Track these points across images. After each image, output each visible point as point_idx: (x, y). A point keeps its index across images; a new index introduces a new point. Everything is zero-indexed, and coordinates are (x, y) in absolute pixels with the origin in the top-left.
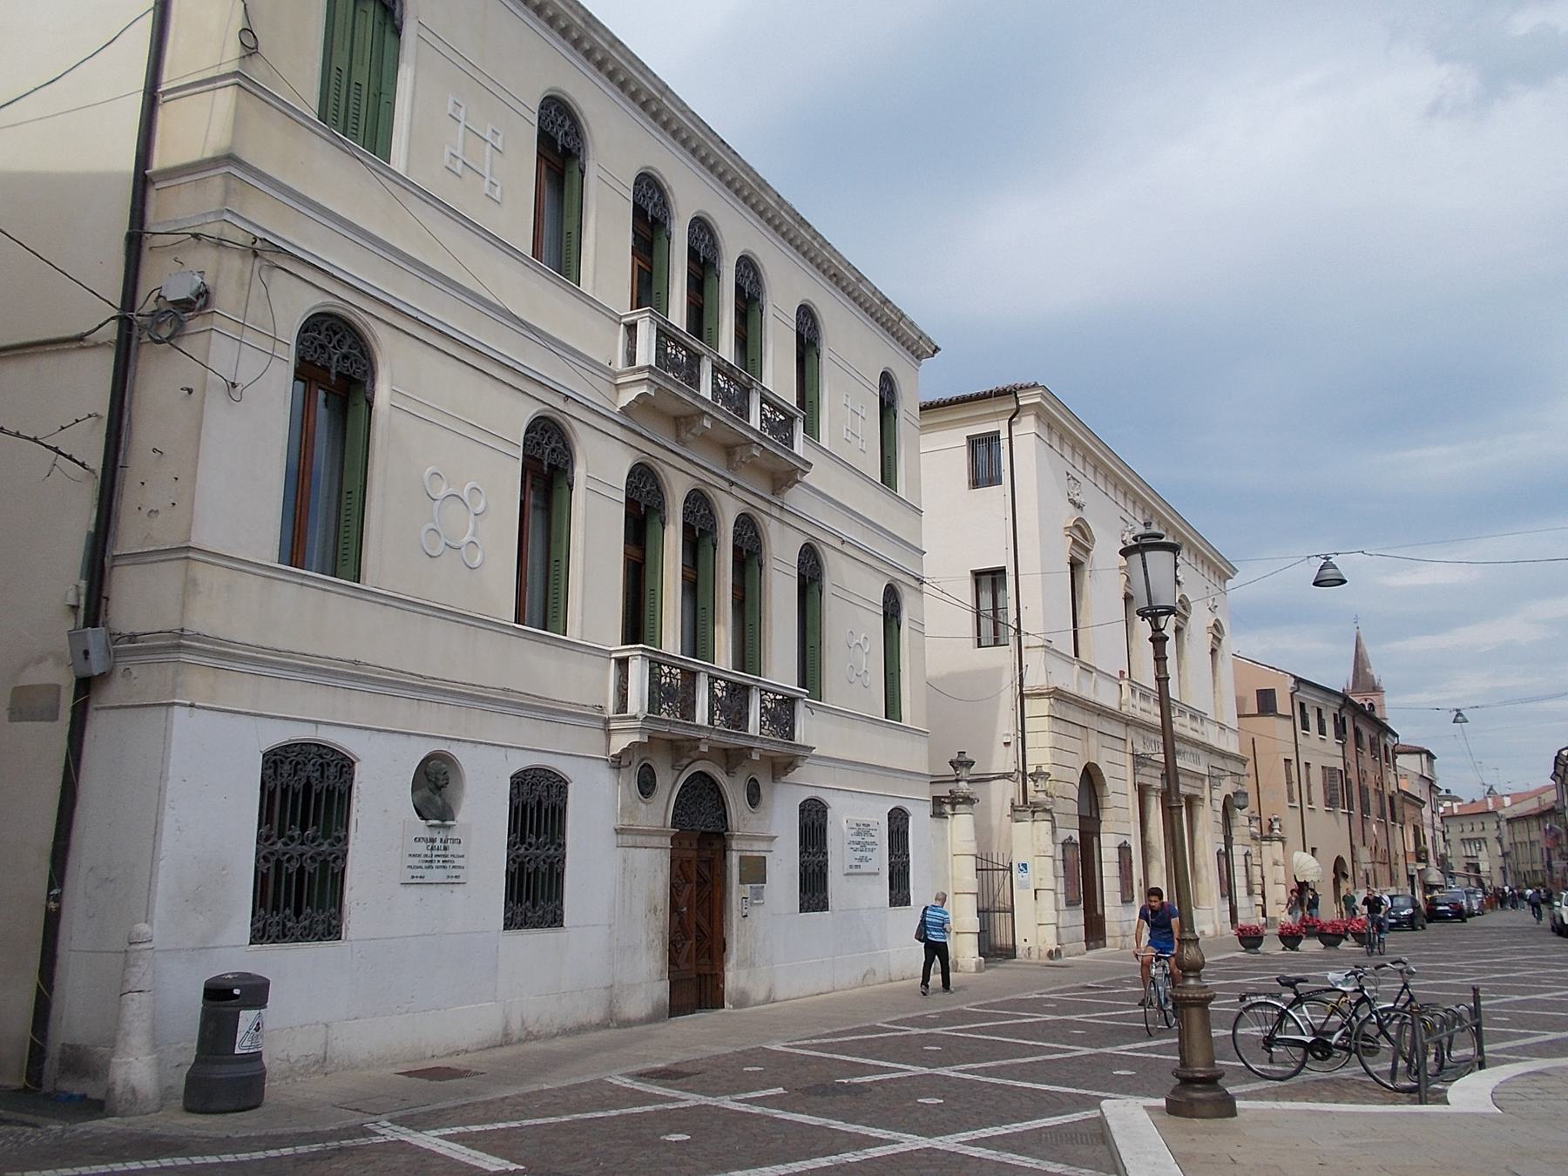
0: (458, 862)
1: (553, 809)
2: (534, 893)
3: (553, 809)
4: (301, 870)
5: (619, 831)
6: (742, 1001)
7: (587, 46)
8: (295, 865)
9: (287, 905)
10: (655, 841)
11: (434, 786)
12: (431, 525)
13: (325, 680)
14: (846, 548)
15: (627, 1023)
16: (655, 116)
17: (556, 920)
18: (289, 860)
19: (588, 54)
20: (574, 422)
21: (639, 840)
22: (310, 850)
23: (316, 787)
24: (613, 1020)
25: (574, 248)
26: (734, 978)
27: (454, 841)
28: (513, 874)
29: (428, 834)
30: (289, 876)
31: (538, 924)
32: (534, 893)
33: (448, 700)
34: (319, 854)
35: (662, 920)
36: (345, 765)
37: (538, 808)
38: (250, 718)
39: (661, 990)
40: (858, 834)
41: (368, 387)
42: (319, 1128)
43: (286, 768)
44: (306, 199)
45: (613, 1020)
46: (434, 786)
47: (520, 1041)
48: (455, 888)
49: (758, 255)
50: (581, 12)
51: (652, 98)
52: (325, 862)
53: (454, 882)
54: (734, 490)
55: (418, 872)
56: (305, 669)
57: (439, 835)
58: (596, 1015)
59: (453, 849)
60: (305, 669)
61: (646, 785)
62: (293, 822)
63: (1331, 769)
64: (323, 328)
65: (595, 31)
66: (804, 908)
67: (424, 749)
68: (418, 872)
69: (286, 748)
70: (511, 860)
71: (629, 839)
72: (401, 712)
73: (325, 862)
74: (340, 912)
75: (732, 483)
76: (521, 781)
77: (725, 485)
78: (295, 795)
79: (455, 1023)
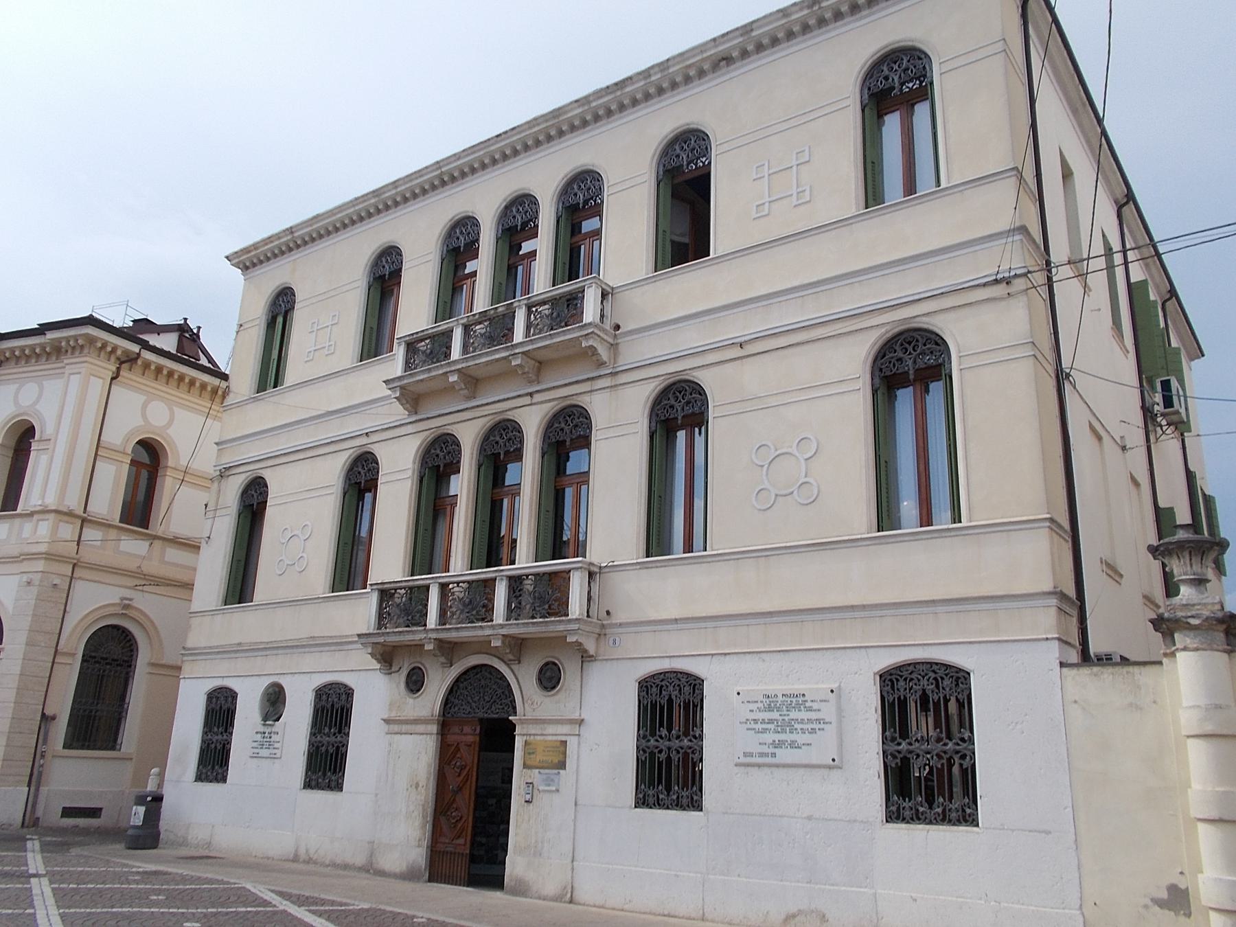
0: (276, 745)
1: (342, 709)
2: (326, 766)
3: (342, 709)
4: (669, 759)
6: (521, 890)
7: (828, 15)
8: (663, 756)
9: (660, 782)
10: (421, 728)
11: (274, 701)
15: (382, 873)
16: (453, 179)
17: (339, 787)
18: (660, 752)
19: (396, 204)
20: (917, 319)
21: (404, 728)
22: (676, 744)
23: (336, 706)
24: (370, 869)
25: (366, 342)
26: (515, 865)
28: (644, 763)
29: (262, 729)
30: (660, 763)
32: (326, 766)
33: (280, 652)
35: (425, 794)
36: (695, 684)
37: (333, 710)
38: (1010, 644)
39: (418, 855)
40: (769, 709)
42: (323, 896)
45: (370, 869)
46: (274, 701)
47: (304, 861)
50: (772, 18)
51: (440, 177)
52: (686, 754)
53: (273, 757)
54: (537, 398)
56: (218, 653)
57: (268, 730)
58: (360, 860)
59: (275, 738)
60: (218, 653)
61: (415, 683)
62: (661, 725)
63: (679, 244)
64: (897, 348)
66: (310, 784)
67: (267, 681)
69: (900, 668)
70: (311, 744)
71: (396, 728)
73: (686, 754)
75: (531, 394)
76: (323, 693)
77: (527, 400)
78: (662, 708)
79: (273, 840)
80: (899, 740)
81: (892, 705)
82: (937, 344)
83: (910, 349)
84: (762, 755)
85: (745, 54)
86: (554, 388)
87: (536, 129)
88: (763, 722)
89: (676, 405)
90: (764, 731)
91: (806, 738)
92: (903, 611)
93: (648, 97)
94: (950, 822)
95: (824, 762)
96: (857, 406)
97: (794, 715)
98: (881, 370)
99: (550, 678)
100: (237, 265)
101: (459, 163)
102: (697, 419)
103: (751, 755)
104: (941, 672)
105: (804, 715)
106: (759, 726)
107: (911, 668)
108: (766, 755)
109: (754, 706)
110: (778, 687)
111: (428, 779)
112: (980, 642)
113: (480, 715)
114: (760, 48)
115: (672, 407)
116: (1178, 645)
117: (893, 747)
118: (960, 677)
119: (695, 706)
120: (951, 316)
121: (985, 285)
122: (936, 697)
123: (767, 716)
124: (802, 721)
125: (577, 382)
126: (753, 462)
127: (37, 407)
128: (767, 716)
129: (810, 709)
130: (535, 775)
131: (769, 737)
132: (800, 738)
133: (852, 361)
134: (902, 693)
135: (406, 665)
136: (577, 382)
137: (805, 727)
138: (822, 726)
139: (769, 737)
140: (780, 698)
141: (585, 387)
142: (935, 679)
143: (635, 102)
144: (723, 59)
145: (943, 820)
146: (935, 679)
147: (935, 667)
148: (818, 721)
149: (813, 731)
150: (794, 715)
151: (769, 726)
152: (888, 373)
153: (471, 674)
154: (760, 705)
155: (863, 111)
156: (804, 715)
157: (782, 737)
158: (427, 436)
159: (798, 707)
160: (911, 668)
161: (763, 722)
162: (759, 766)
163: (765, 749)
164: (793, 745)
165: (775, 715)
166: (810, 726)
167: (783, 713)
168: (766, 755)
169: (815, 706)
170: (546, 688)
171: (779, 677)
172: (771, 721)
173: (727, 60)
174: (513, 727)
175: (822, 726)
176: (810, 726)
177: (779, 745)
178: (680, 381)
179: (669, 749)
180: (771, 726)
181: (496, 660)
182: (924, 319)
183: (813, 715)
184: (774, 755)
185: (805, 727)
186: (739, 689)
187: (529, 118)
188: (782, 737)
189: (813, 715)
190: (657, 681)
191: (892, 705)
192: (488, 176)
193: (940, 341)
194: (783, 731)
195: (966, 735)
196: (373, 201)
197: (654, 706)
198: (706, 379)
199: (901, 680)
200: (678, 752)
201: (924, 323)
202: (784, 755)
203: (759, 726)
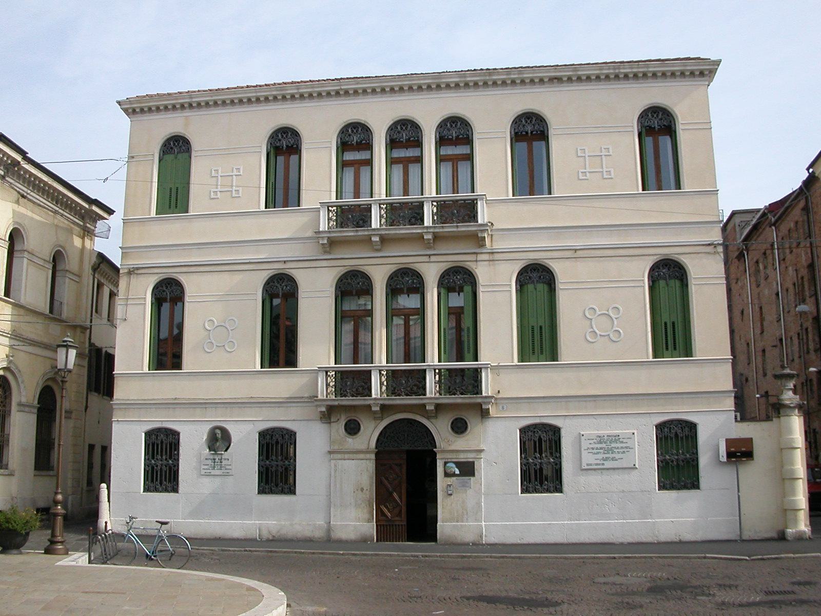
0: (228, 467)
4: (277, 471)
5: (330, 453)
8: (273, 469)
10: (368, 456)
11: (219, 440)
12: (209, 341)
13: (268, 405)
14: (580, 253)
27: (225, 459)
29: (212, 457)
31: (685, 487)
34: (284, 465)
39: (370, 529)
41: (296, 295)
43: (268, 437)
44: (245, 241)
46: (219, 440)
48: (229, 477)
49: (172, 131)
54: (433, 259)
55: (209, 471)
61: (352, 428)
62: (157, 454)
65: (286, 90)
68: (209, 471)
69: (268, 430)
72: (198, 415)
74: (178, 484)
75: (429, 256)
77: (426, 259)
80: (284, 460)
84: (597, 464)
85: (570, 79)
86: (389, 257)
88: (597, 449)
90: (598, 453)
91: (620, 456)
92: (667, 397)
93: (504, 83)
94: (285, 493)
95: (630, 466)
97: (613, 445)
98: (390, 285)
99: (459, 427)
100: (126, 111)
103: (591, 465)
104: (684, 425)
105: (619, 445)
106: (595, 451)
108: (599, 464)
109: (592, 442)
111: (371, 485)
112: (617, 414)
113: (406, 447)
114: (579, 79)
115: (164, 291)
116: (332, 420)
117: (262, 463)
119: (175, 445)
121: (703, 245)
123: (599, 446)
124: (618, 448)
126: (204, 325)
127: (469, 146)
128: (599, 446)
129: (622, 442)
130: (450, 480)
131: (600, 456)
132: (617, 456)
133: (641, 270)
134: (687, 433)
138: (628, 450)
139: (600, 456)
141: (472, 257)
142: (682, 428)
143: (495, 83)
144: (556, 78)
145: (282, 492)
146: (282, 435)
147: (681, 422)
148: (626, 447)
149: (624, 452)
150: (613, 445)
152: (158, 297)
154: (595, 441)
156: (619, 445)
157: (607, 455)
158: (341, 271)
159: (616, 441)
160: (670, 423)
161: (597, 449)
162: (595, 470)
163: (598, 462)
164: (613, 459)
165: (604, 445)
166: (622, 450)
167: (609, 445)
168: (599, 464)
169: (625, 441)
170: (457, 432)
171: (607, 429)
172: (601, 448)
173: (559, 79)
174: (435, 454)
175: (628, 450)
176: (622, 450)
177: (606, 459)
178: (536, 264)
179: (277, 465)
180: (602, 451)
182: (174, 274)
183: (624, 445)
184: (603, 464)
186: (636, 434)
187: (215, 87)
188: (607, 455)
189: (624, 445)
190: (270, 433)
192: (628, 86)
195: (558, 455)
196: (274, 93)
197: (268, 444)
200: (282, 467)
201: (362, 269)
202: (608, 464)
203: (595, 451)
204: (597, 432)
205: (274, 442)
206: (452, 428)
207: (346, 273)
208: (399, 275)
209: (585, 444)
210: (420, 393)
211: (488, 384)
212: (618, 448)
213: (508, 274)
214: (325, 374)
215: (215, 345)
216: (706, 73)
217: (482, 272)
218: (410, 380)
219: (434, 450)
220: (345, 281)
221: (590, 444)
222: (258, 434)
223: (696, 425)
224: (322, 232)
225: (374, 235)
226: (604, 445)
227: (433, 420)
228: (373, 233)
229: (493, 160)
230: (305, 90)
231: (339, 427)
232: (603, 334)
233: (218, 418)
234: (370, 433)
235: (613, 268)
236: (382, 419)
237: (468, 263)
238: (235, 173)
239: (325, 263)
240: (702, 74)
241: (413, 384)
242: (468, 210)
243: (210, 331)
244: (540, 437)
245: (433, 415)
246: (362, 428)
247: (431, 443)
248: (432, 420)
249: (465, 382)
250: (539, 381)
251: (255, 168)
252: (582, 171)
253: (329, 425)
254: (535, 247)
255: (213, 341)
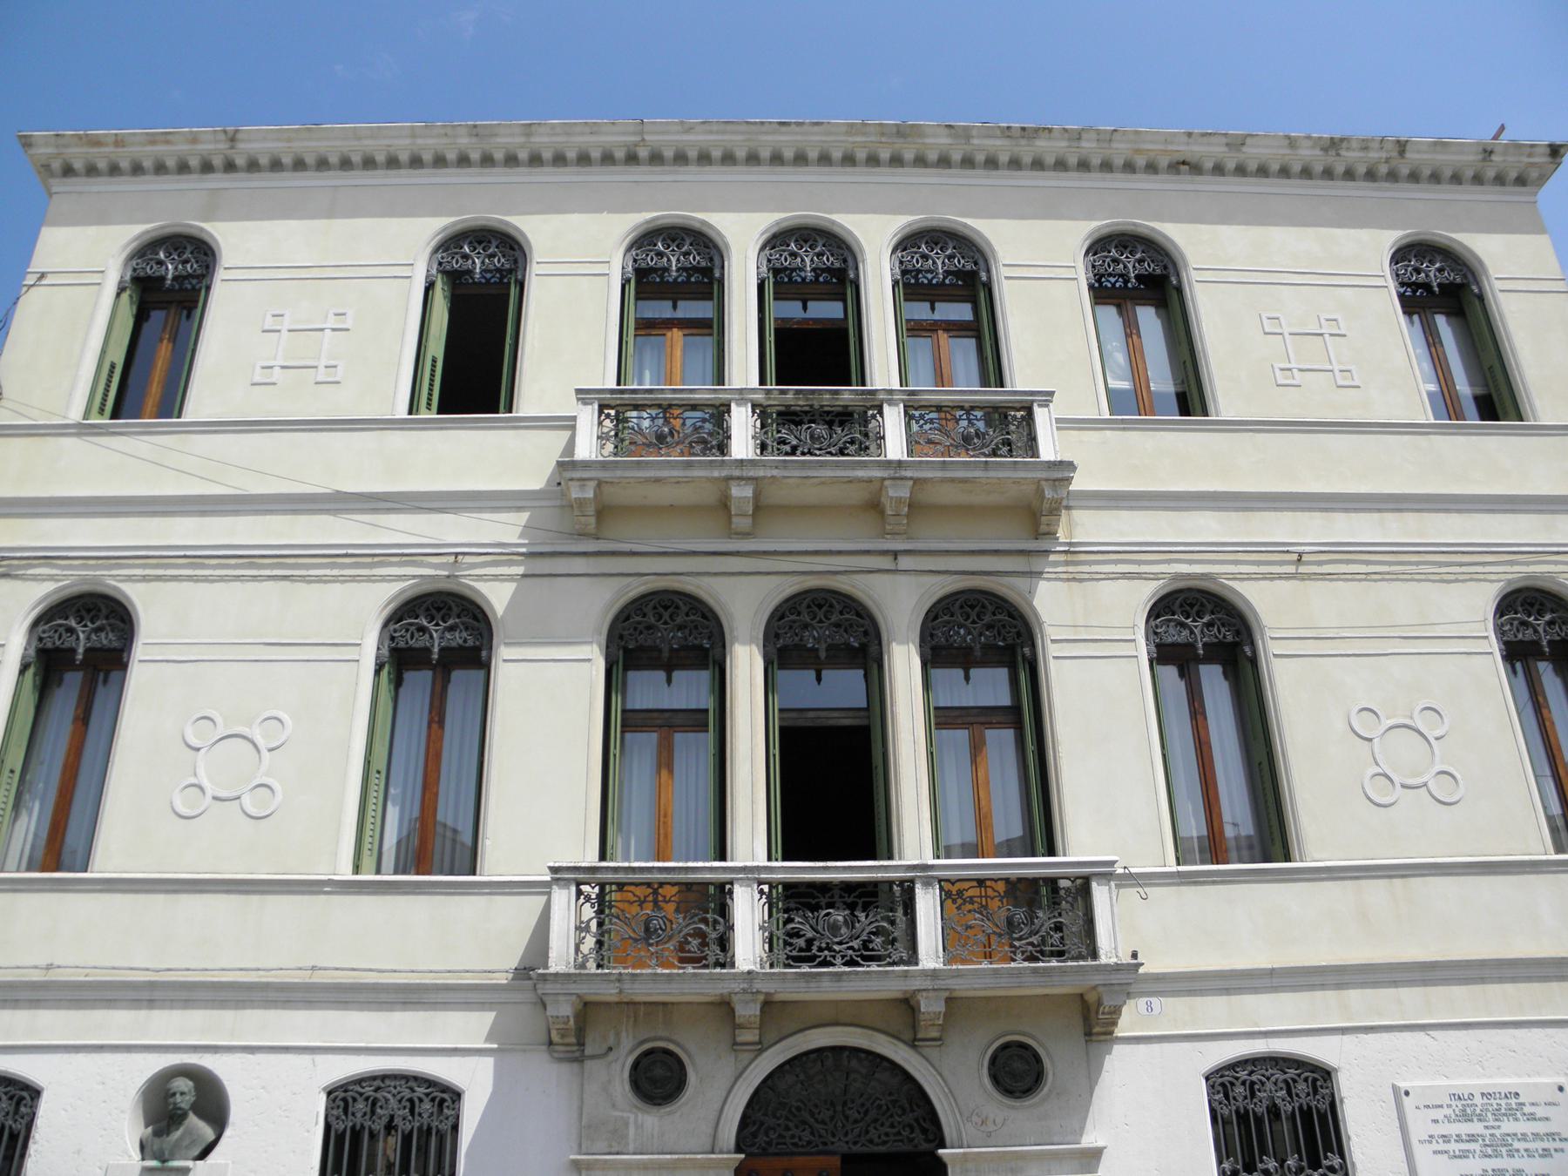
12: (193, 780)
40: (1465, 1117)
54: (905, 562)
61: (658, 1079)
64: (803, 608)
69: (360, 1081)
75: (895, 554)
81: (340, 1138)
82: (704, 617)
83: (666, 616)
87: (859, 139)
88: (1459, 1139)
89: (79, 629)
90: (1464, 1155)
93: (1061, 165)
96: (355, 682)
97: (1508, 1126)
99: (1017, 1072)
101: (685, 137)
102: (109, 662)
105: (1523, 1127)
106: (1454, 1147)
107: (378, 1083)
109: (1438, 1114)
110: (1472, 1082)
116: (588, 1051)
118: (1320, 1075)
120: (141, 586)
122: (1290, 1108)
123: (1465, 1128)
124: (1524, 1138)
125: (996, 552)
128: (1465, 1128)
129: (1532, 1117)
133: (360, 615)
134: (359, 1120)
135: (627, 1042)
136: (996, 552)
137: (1531, 1146)
138: (1558, 1145)
140: (1478, 1100)
146: (411, 1100)
148: (1552, 1136)
150: (1508, 1126)
151: (1471, 1146)
153: (885, 1064)
154: (1449, 1112)
155: (118, 295)
156: (1523, 1127)
159: (1511, 1114)
160: (378, 1083)
161: (1459, 1139)
165: (1476, 1128)
166: (1539, 1145)
169: (1540, 1112)
172: (1472, 1138)
175: (1558, 1145)
176: (1539, 1145)
181: (882, 1038)
185: (1531, 1146)
189: (1540, 1128)
191: (340, 1138)
193: (480, 616)
194: (1498, 1155)
195: (1336, 1161)
197: (1243, 1117)
198: (140, 597)
199: (360, 1099)
201: (842, 584)
203: (1454, 1147)
204: (1444, 1082)
205: (379, 1126)
206: (996, 1079)
207: (643, 596)
208: (803, 608)
209: (1420, 1126)
210: (895, 957)
211: (1118, 925)
212: (1524, 1138)
213: (1126, 607)
214: (573, 888)
215: (209, 793)
216: (1534, 174)
217: (1053, 605)
218: (862, 916)
219: (941, 1151)
220: (639, 619)
221: (1435, 1121)
222: (323, 1097)
223: (1329, 1073)
224: (586, 465)
225: (740, 478)
226: (1476, 1128)
227: (932, 1053)
228: (737, 473)
229: (1052, 333)
230: (546, 139)
231: (616, 1075)
232: (1410, 782)
233: (180, 1032)
234: (720, 1095)
235: (1402, 602)
236: (761, 1047)
237: (1006, 580)
238: (332, 322)
239: (579, 565)
240: (1521, 181)
241: (871, 928)
242: (1009, 424)
243: (198, 750)
244: (392, 1117)
245: (935, 1034)
246: (692, 1077)
247: (924, 1131)
248: (926, 1051)
249: (1046, 910)
250: (1243, 920)
251: (334, 701)
252: (1283, 366)
253: (575, 1066)
254: (1199, 543)
255: (206, 783)
